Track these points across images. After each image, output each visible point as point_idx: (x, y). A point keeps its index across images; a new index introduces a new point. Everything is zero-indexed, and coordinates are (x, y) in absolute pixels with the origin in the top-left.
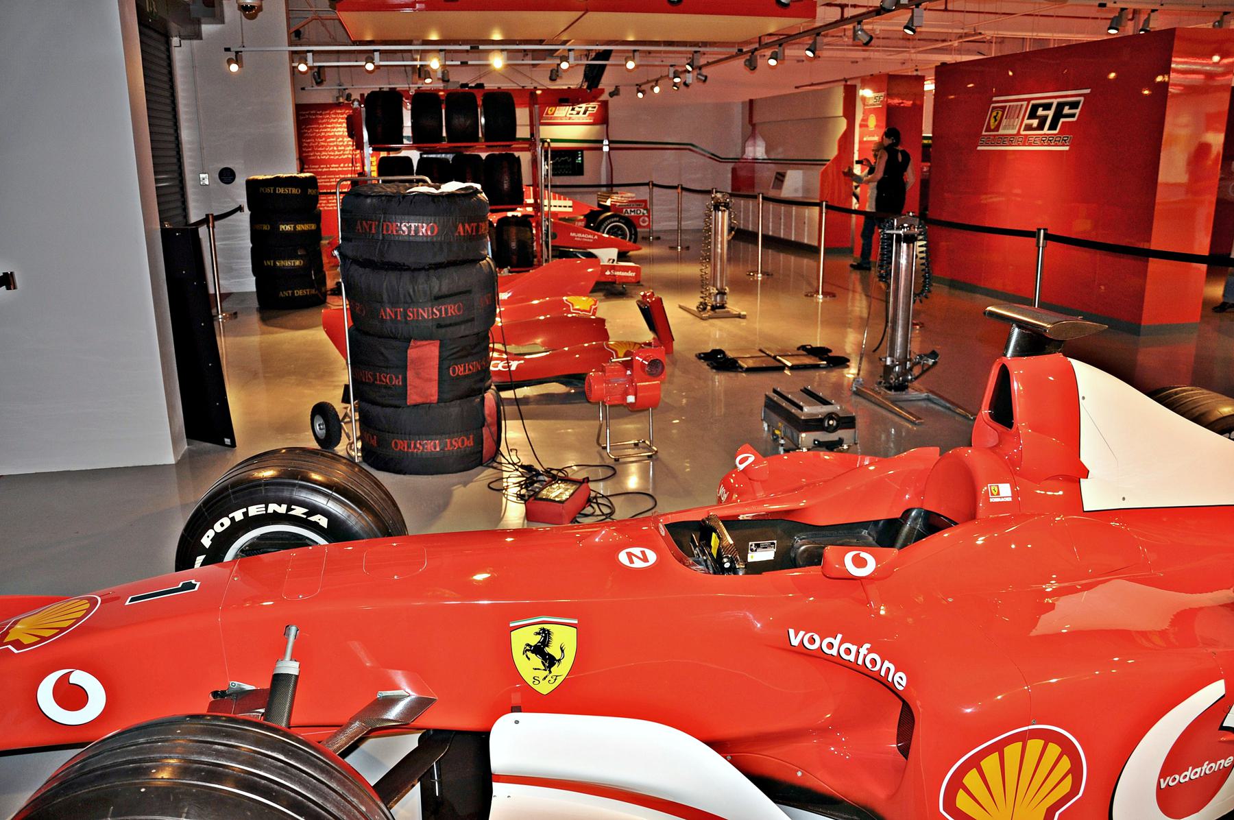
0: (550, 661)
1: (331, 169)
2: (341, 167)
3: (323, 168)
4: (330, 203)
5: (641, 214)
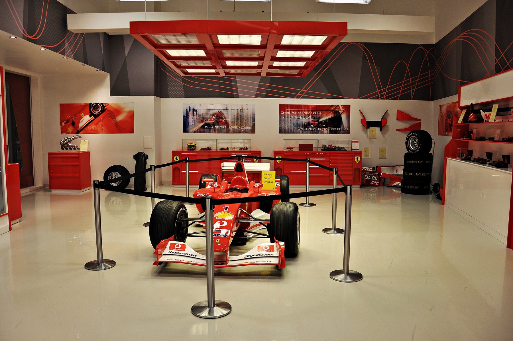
5: (374, 179)
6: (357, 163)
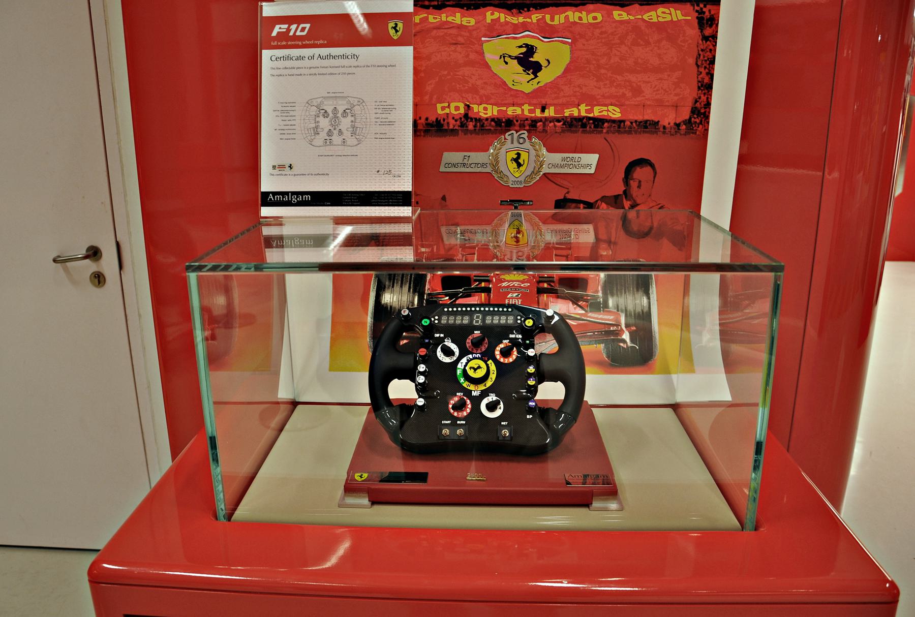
0: (397, 31)
6: (395, 38)
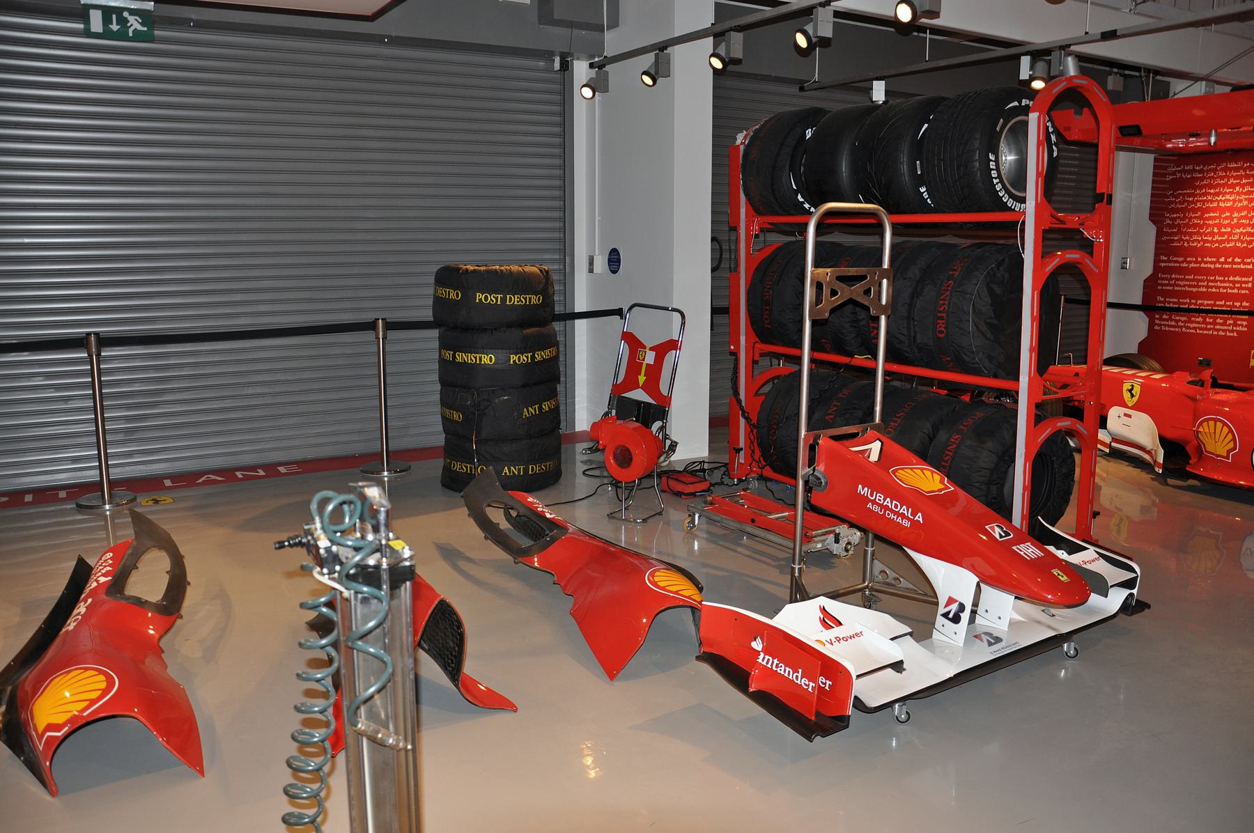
1: (1203, 265)
2: (1220, 263)
3: (1190, 262)
4: (1192, 322)
